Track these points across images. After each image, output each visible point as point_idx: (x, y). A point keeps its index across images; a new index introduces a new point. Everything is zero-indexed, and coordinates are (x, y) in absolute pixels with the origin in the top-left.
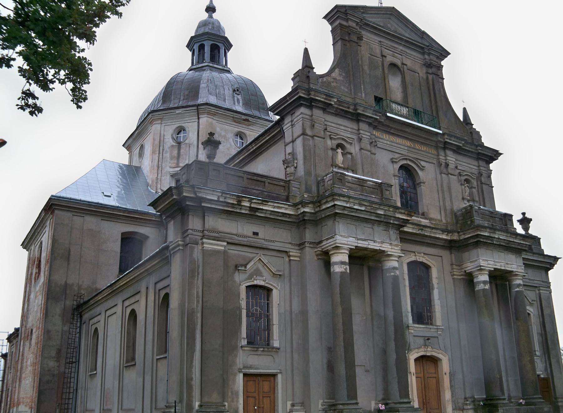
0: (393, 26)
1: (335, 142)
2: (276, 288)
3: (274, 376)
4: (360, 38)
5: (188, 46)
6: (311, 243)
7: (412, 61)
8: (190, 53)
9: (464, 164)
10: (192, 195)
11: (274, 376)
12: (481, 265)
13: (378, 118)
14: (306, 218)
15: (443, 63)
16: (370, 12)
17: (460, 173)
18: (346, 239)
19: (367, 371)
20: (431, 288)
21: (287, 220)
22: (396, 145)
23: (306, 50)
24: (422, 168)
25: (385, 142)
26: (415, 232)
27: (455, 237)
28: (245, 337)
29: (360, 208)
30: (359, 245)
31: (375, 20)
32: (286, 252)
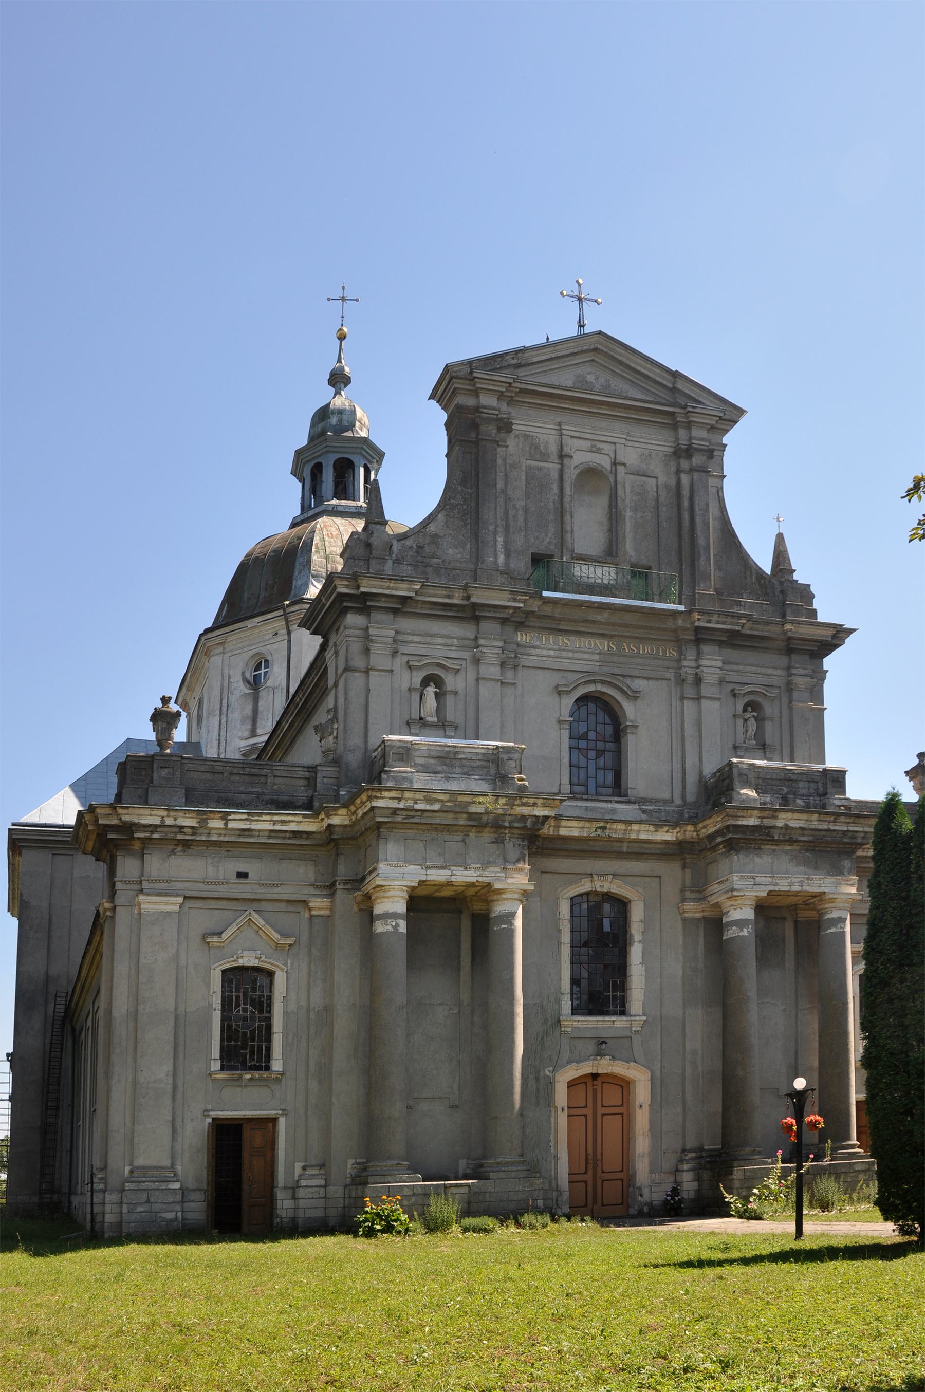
2: (282, 970)
3: (274, 1120)
4: (506, 426)
6: (346, 882)
7: (639, 451)
8: (300, 485)
10: (115, 822)
11: (274, 1120)
12: (735, 887)
13: (521, 605)
14: (335, 837)
15: (725, 440)
16: (535, 360)
17: (733, 690)
18: (396, 878)
19: (454, 1107)
20: (628, 942)
21: (304, 843)
22: (570, 655)
23: (780, 538)
25: (545, 652)
27: (689, 832)
28: (218, 1056)
29: (428, 807)
32: (305, 902)
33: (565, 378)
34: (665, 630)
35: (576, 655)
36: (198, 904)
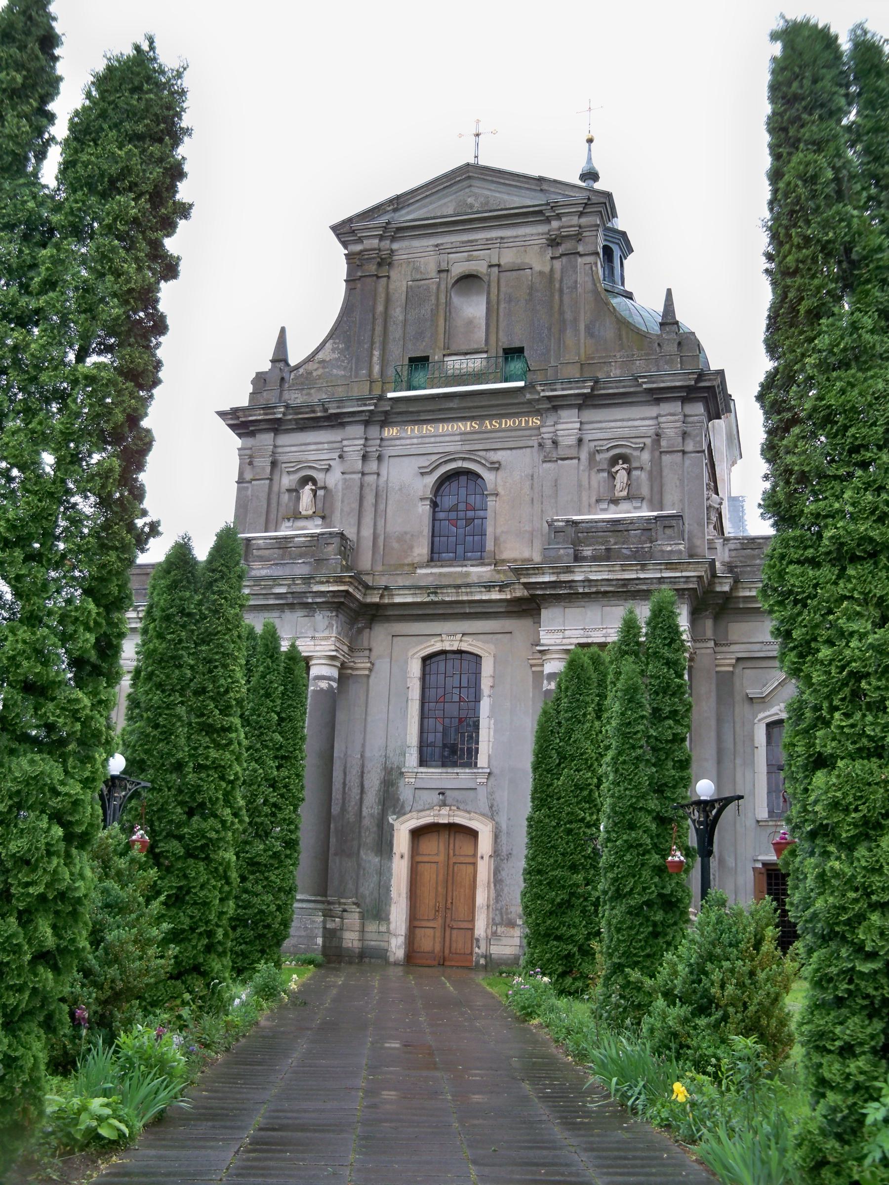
0: (481, 196)
1: (297, 477)
9: (613, 424)
22: (432, 440)
23: (283, 331)
24: (496, 467)
25: (408, 441)
31: (425, 210)
33: (445, 207)
35: (438, 439)
36: (749, 664)
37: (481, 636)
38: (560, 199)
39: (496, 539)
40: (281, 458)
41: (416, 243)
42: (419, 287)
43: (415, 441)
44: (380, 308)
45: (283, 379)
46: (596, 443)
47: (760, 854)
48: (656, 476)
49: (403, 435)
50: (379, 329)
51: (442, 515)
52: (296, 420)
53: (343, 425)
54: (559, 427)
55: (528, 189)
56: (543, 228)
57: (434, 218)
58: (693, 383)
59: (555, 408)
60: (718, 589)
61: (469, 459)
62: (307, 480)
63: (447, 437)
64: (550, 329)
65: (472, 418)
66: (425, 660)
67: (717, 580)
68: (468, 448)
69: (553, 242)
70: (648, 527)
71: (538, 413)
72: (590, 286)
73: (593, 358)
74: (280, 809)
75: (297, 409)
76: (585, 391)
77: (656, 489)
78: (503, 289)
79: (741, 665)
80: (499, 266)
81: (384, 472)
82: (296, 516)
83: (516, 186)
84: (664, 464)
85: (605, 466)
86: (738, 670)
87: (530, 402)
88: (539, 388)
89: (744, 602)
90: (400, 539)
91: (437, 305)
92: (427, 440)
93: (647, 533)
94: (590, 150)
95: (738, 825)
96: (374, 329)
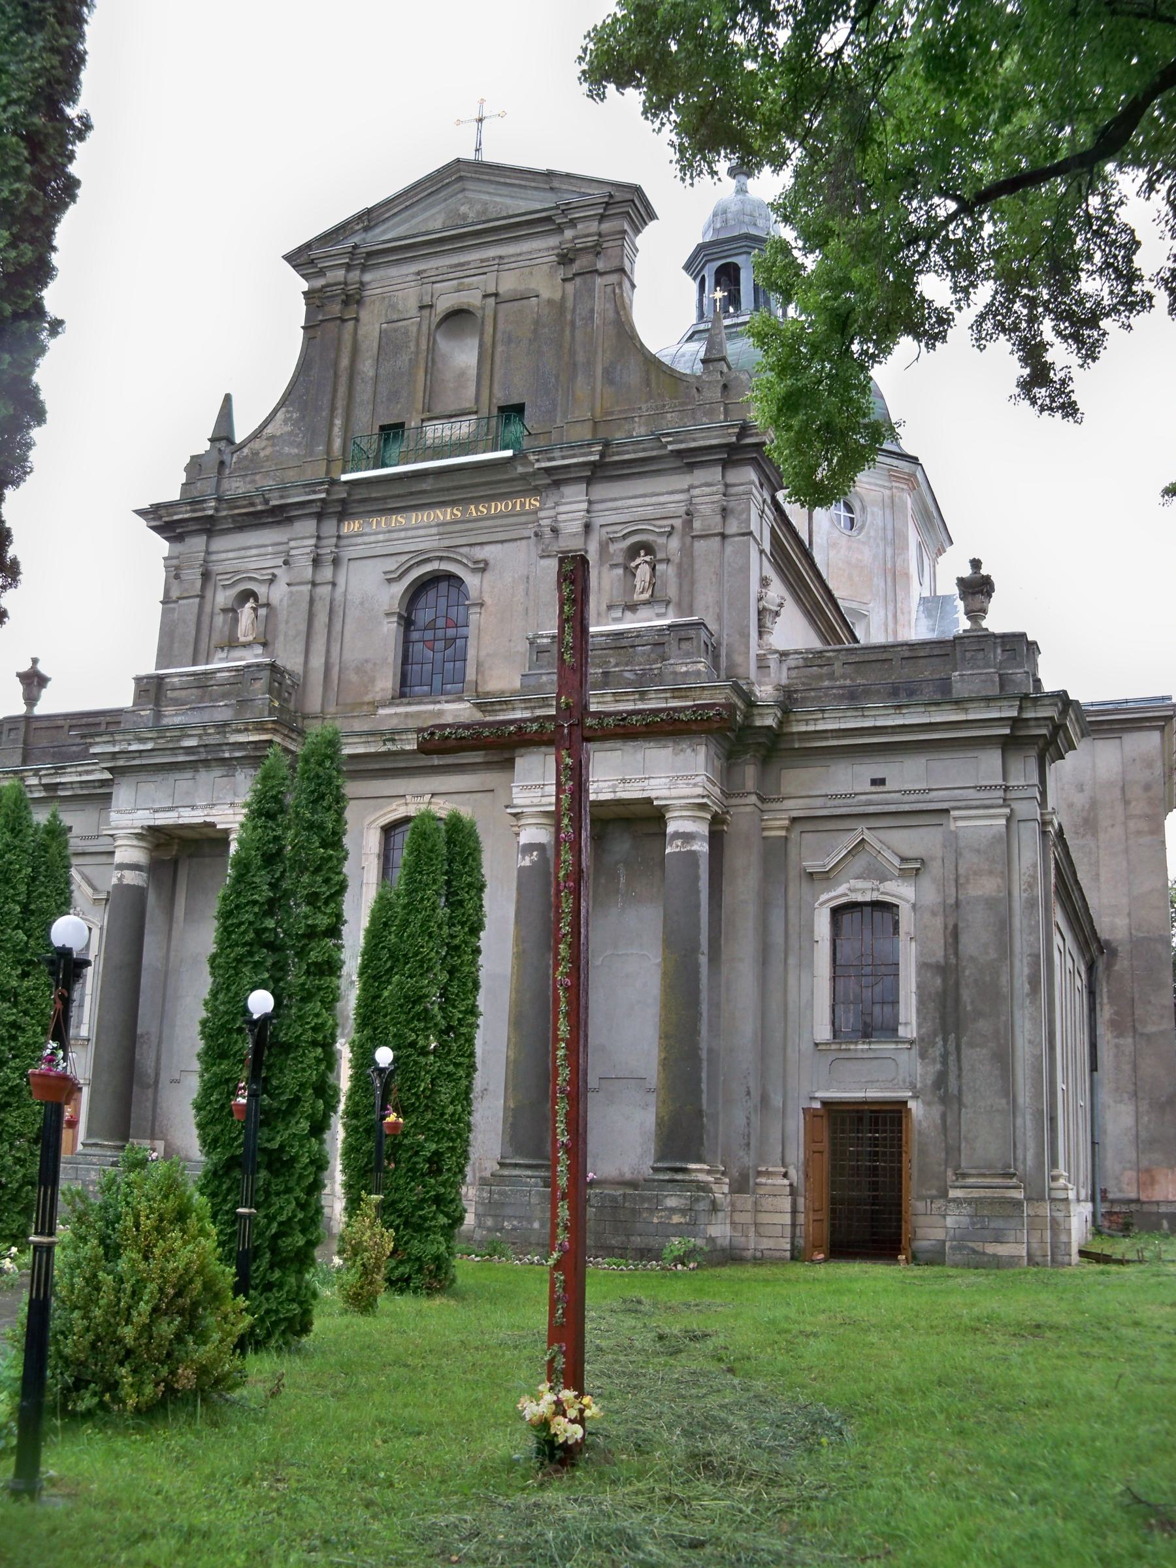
5: (687, 267)
8: (694, 286)
9: (632, 502)
22: (403, 534)
23: (228, 399)
24: (482, 567)
25: (373, 538)
26: (372, 749)
29: (142, 747)
30: (158, 823)
31: (406, 226)
33: (432, 219)
34: (513, 480)
35: (410, 534)
36: (809, 826)
37: (456, 797)
38: (574, 199)
39: (479, 665)
40: (216, 568)
41: (393, 271)
42: (396, 330)
43: (381, 537)
44: (345, 362)
45: (222, 463)
46: (609, 529)
47: (818, 1090)
48: (686, 572)
49: (367, 530)
50: (342, 390)
51: (415, 635)
52: (232, 516)
53: (290, 520)
54: (562, 509)
55: (535, 188)
56: (553, 241)
57: (414, 236)
58: (734, 439)
59: (557, 484)
60: (758, 723)
61: (448, 559)
62: (247, 595)
63: (418, 531)
64: (557, 377)
65: (453, 503)
66: (388, 830)
67: (755, 711)
68: (447, 543)
69: (565, 259)
70: (659, 641)
71: (536, 491)
72: (611, 314)
73: (612, 413)
74: (24, 1030)
75: (232, 503)
76: (592, 458)
77: (686, 588)
78: (501, 326)
79: (799, 827)
80: (496, 295)
81: (341, 581)
82: (232, 643)
83: (520, 186)
84: (696, 554)
85: (620, 560)
86: (794, 836)
87: (524, 477)
88: (532, 458)
89: (800, 740)
90: (358, 670)
91: (417, 353)
92: (395, 535)
93: (659, 650)
94: (479, 131)
95: (789, 1050)
96: (335, 391)
